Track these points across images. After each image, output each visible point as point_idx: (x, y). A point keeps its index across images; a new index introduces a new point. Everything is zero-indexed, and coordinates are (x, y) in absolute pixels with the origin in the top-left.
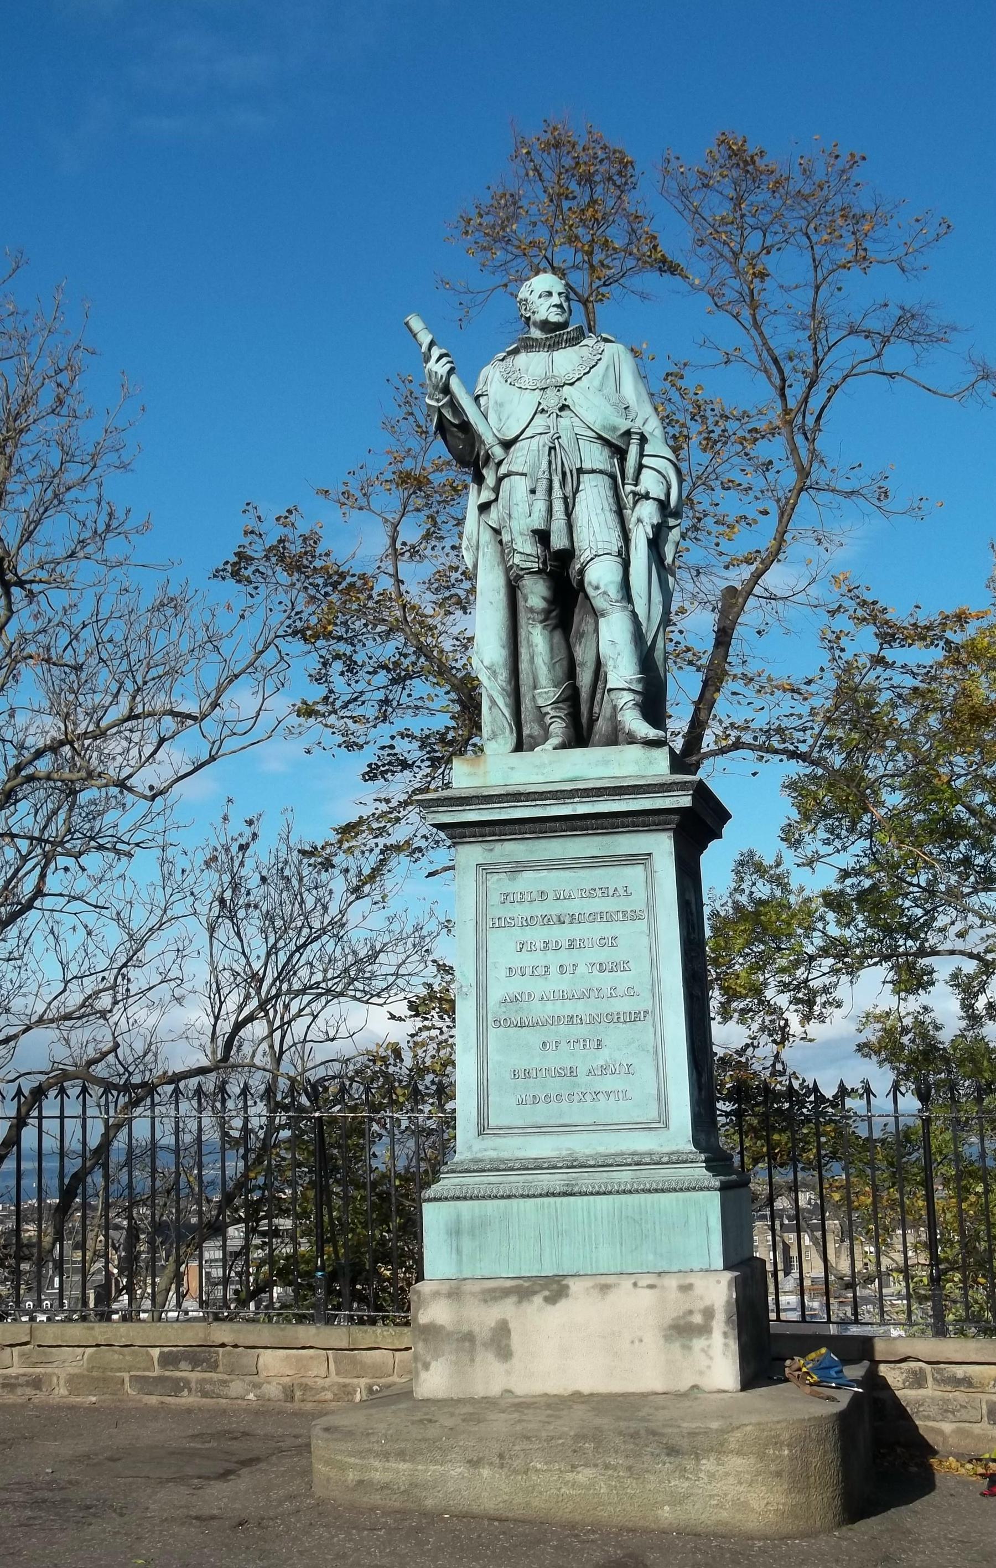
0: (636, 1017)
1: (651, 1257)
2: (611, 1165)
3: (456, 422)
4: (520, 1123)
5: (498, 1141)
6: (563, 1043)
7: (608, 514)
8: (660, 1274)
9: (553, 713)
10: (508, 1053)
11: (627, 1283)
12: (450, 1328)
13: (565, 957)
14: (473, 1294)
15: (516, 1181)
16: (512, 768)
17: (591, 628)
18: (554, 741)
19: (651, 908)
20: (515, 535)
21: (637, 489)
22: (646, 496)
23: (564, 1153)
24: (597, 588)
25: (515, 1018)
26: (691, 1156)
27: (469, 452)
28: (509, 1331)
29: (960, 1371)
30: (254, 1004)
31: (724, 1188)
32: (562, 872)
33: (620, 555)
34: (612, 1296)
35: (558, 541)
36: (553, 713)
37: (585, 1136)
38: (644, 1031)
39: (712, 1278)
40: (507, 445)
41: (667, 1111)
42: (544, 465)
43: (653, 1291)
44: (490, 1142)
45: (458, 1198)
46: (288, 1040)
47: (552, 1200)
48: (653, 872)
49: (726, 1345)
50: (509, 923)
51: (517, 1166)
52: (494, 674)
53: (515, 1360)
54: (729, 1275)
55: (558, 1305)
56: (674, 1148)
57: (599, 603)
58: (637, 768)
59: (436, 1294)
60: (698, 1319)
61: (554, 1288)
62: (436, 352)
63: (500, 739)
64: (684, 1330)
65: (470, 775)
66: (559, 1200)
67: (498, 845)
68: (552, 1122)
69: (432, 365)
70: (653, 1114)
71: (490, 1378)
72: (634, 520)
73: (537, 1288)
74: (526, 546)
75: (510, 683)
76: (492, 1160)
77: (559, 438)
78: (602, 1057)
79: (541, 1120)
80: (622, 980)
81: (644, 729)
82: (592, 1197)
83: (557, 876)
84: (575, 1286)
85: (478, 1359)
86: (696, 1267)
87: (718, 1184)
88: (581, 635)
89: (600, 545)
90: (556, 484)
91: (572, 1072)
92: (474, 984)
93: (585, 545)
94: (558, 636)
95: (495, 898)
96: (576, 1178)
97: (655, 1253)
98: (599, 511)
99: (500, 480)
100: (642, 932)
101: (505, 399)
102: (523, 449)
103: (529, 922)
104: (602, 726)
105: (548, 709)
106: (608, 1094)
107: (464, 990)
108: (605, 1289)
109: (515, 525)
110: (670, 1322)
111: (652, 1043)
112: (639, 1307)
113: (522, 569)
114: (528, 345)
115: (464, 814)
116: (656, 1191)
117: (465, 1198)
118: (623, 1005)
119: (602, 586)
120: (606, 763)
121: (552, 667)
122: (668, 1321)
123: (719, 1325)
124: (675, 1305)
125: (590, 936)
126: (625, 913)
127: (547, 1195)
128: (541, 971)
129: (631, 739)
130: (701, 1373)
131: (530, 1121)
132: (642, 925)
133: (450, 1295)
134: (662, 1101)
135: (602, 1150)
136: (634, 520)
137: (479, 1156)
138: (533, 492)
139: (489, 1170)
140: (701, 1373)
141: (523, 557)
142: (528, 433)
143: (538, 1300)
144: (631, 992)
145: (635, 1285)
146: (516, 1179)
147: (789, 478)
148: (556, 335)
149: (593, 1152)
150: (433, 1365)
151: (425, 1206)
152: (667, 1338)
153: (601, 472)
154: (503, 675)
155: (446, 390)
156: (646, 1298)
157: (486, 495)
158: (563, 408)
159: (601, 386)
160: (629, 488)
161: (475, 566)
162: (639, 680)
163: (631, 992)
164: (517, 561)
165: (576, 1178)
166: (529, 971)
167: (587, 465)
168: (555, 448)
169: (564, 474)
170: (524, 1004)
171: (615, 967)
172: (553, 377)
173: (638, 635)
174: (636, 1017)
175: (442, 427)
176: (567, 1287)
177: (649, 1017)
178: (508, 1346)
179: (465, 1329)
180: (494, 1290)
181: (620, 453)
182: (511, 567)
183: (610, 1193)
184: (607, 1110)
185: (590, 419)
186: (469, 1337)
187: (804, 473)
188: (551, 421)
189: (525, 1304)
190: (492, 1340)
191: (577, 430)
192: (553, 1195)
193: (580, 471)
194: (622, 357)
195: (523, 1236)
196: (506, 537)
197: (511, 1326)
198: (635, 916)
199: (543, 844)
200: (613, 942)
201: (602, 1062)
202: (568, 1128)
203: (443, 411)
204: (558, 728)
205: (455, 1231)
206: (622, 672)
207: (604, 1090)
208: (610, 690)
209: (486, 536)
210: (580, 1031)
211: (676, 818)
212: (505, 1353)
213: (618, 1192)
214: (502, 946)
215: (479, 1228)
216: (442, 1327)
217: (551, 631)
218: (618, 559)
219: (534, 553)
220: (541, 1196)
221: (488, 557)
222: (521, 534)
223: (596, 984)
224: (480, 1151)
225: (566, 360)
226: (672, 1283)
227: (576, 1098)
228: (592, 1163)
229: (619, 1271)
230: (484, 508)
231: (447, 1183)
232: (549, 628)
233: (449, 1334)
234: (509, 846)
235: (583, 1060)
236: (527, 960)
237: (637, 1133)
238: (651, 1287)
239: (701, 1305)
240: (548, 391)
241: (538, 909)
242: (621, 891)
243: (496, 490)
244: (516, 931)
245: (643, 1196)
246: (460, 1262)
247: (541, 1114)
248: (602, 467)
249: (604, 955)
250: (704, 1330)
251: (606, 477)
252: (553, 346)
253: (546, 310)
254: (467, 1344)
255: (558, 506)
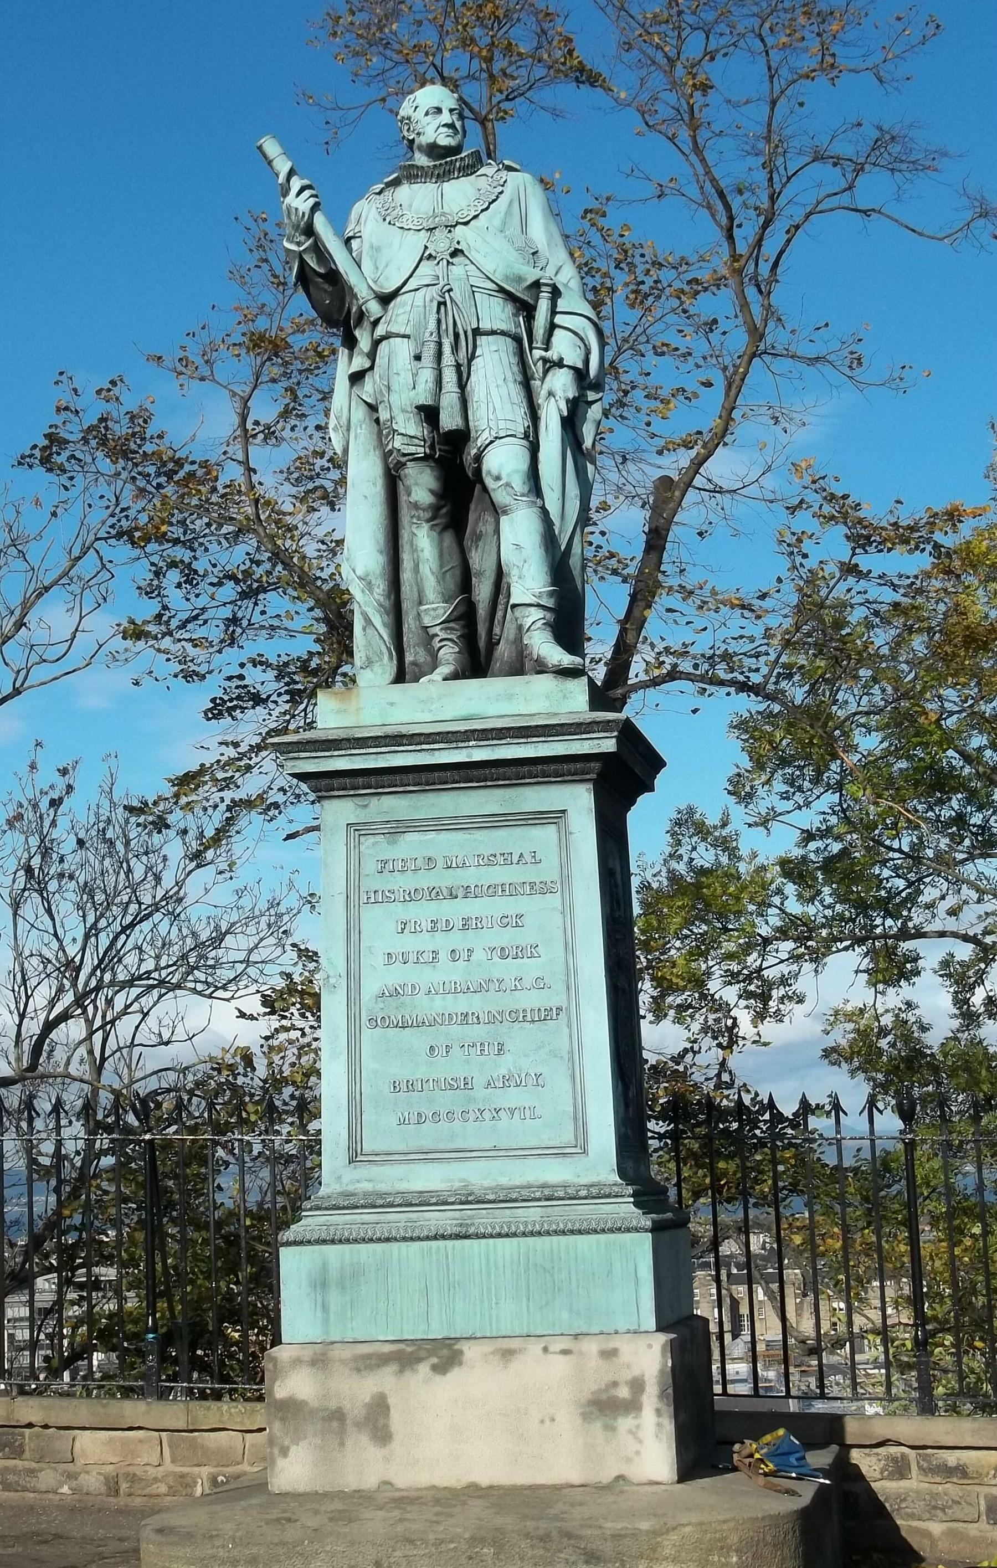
0: (547, 1015)
1: (565, 1315)
2: (515, 1200)
3: (322, 271)
4: (402, 1147)
5: (375, 1170)
6: (456, 1048)
7: (511, 385)
8: (576, 1336)
9: (443, 635)
10: (386, 1057)
11: (535, 1348)
12: (314, 1403)
13: (457, 940)
14: (343, 1362)
15: (396, 1219)
16: (392, 704)
17: (490, 528)
18: (445, 670)
19: (566, 878)
20: (396, 411)
21: (548, 354)
22: (560, 364)
23: (457, 1185)
24: (498, 478)
25: (396, 1016)
26: (616, 1189)
27: (338, 309)
28: (388, 1408)
29: (952, 1458)
30: (68, 998)
31: (656, 1229)
32: (461, 833)
33: (526, 436)
34: (517, 1364)
35: (449, 420)
36: (443, 635)
37: (482, 1164)
38: (557, 1032)
39: (642, 1341)
40: (386, 299)
41: (585, 1133)
42: (432, 325)
43: (568, 1357)
44: (363, 1172)
45: (324, 1242)
46: (112, 1044)
47: (441, 1243)
48: (568, 833)
49: (659, 1425)
50: (387, 898)
51: (398, 1201)
52: (369, 585)
53: (395, 1444)
54: (663, 1338)
55: (449, 1375)
56: (594, 1179)
57: (500, 497)
58: (547, 704)
59: (297, 1362)
60: (623, 1392)
61: (444, 1354)
62: (296, 183)
63: (377, 668)
64: (606, 1407)
65: (338, 712)
66: (450, 1243)
67: (374, 800)
68: (442, 1146)
69: (291, 200)
70: (567, 1136)
71: (364, 1466)
72: (544, 393)
73: (423, 1354)
74: (409, 427)
75: (389, 597)
76: (366, 1194)
77: (450, 290)
78: (505, 1065)
79: (428, 1144)
80: (530, 968)
81: (557, 655)
82: (491, 1241)
83: (448, 838)
84: (470, 1352)
85: (349, 1443)
86: (622, 1327)
87: (649, 1223)
88: (478, 537)
89: (502, 425)
90: (447, 349)
91: (467, 1084)
92: (344, 974)
93: (482, 424)
94: (449, 538)
95: (370, 866)
96: (471, 1216)
97: (571, 1310)
98: (501, 382)
99: (376, 343)
100: (554, 909)
101: (383, 243)
102: (405, 304)
103: (412, 896)
104: (504, 651)
105: (437, 630)
106: (512, 1111)
107: (332, 981)
108: (508, 1354)
109: (395, 399)
110: (590, 1397)
111: (566, 1048)
112: (551, 1378)
113: (405, 455)
114: (412, 174)
115: (331, 761)
116: (572, 1232)
117: (333, 1242)
118: (530, 1000)
119: (504, 475)
120: (510, 697)
121: (441, 578)
122: (586, 1396)
123: (651, 1399)
124: (596, 1375)
125: (490, 914)
126: (532, 885)
127: (435, 1238)
128: (428, 957)
129: (541, 668)
130: (628, 1460)
131: (414, 1145)
132: (554, 900)
133: (313, 1363)
134: (579, 1120)
135: (504, 1181)
136: (544, 393)
137: (351, 1188)
138: (418, 358)
139: (363, 1207)
140: (628, 1460)
141: (406, 440)
142: (411, 285)
143: (424, 1369)
144: (540, 984)
145: (545, 1350)
146: (395, 1217)
147: (739, 340)
148: (446, 162)
149: (494, 1184)
150: (293, 1450)
151: (283, 1251)
152: (586, 1417)
153: (503, 333)
154: (380, 587)
155: (309, 231)
156: (559, 1366)
157: (359, 362)
158: (456, 253)
159: (501, 225)
160: (538, 353)
161: (346, 451)
162: (551, 594)
163: (540, 984)
164: (397, 444)
165: (471, 1216)
166: (412, 958)
167: (485, 325)
168: (445, 303)
169: (456, 336)
170: (407, 999)
171: (520, 953)
172: (443, 214)
173: (549, 537)
174: (547, 1015)
175: (304, 277)
176: (461, 1352)
177: (563, 1015)
178: (386, 1426)
179: (333, 1405)
180: (369, 1356)
181: (526, 309)
182: (391, 452)
183: (515, 1235)
184: (511, 1131)
185: (488, 268)
186: (338, 1416)
187: (756, 334)
188: (441, 270)
189: (408, 1374)
190: (367, 1419)
191: (473, 281)
192: (443, 1237)
193: (477, 332)
194: (529, 190)
195: (406, 1289)
196: (384, 415)
197: (391, 1401)
198: (544, 889)
199: (431, 798)
200: (517, 921)
201: (504, 1071)
202: (462, 1154)
203: (305, 257)
204: (449, 654)
205: (321, 1283)
206: (529, 583)
207: (507, 1107)
208: (514, 606)
209: (359, 413)
210: (476, 1032)
211: (596, 766)
212: (382, 1436)
213: (524, 1234)
214: (379, 926)
215: (350, 1279)
216: (304, 1403)
217: (441, 533)
218: (524, 442)
219: (419, 434)
220: (427, 1238)
221: (362, 439)
222: (403, 411)
223: (496, 974)
224: (352, 1182)
225: (459, 194)
226: (592, 1347)
227: (472, 1116)
228: (491, 1197)
229: (525, 1332)
230: (357, 378)
231: (311, 1223)
232: (438, 529)
233: (313, 1412)
234: (388, 801)
235: (480, 1069)
236: (410, 943)
237: (548, 1160)
238: (565, 1352)
239: (628, 1375)
240: (437, 232)
241: (425, 880)
242: (528, 857)
243: (372, 355)
244: (398, 908)
245: (555, 1239)
246: (326, 1321)
247: (428, 1135)
248: (504, 327)
249: (506, 937)
250: (633, 1406)
251: (509, 340)
252: (443, 175)
253: (434, 131)
254: (335, 1424)
255: (449, 376)
